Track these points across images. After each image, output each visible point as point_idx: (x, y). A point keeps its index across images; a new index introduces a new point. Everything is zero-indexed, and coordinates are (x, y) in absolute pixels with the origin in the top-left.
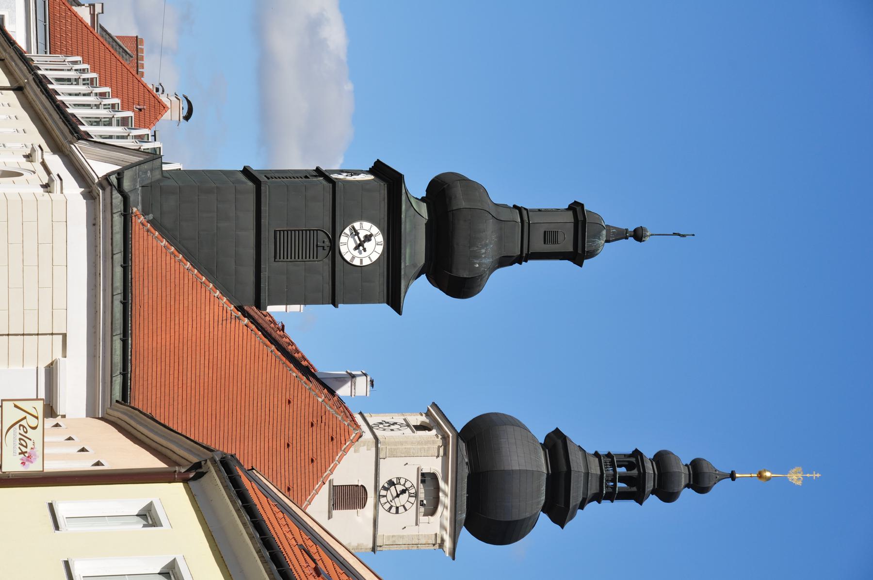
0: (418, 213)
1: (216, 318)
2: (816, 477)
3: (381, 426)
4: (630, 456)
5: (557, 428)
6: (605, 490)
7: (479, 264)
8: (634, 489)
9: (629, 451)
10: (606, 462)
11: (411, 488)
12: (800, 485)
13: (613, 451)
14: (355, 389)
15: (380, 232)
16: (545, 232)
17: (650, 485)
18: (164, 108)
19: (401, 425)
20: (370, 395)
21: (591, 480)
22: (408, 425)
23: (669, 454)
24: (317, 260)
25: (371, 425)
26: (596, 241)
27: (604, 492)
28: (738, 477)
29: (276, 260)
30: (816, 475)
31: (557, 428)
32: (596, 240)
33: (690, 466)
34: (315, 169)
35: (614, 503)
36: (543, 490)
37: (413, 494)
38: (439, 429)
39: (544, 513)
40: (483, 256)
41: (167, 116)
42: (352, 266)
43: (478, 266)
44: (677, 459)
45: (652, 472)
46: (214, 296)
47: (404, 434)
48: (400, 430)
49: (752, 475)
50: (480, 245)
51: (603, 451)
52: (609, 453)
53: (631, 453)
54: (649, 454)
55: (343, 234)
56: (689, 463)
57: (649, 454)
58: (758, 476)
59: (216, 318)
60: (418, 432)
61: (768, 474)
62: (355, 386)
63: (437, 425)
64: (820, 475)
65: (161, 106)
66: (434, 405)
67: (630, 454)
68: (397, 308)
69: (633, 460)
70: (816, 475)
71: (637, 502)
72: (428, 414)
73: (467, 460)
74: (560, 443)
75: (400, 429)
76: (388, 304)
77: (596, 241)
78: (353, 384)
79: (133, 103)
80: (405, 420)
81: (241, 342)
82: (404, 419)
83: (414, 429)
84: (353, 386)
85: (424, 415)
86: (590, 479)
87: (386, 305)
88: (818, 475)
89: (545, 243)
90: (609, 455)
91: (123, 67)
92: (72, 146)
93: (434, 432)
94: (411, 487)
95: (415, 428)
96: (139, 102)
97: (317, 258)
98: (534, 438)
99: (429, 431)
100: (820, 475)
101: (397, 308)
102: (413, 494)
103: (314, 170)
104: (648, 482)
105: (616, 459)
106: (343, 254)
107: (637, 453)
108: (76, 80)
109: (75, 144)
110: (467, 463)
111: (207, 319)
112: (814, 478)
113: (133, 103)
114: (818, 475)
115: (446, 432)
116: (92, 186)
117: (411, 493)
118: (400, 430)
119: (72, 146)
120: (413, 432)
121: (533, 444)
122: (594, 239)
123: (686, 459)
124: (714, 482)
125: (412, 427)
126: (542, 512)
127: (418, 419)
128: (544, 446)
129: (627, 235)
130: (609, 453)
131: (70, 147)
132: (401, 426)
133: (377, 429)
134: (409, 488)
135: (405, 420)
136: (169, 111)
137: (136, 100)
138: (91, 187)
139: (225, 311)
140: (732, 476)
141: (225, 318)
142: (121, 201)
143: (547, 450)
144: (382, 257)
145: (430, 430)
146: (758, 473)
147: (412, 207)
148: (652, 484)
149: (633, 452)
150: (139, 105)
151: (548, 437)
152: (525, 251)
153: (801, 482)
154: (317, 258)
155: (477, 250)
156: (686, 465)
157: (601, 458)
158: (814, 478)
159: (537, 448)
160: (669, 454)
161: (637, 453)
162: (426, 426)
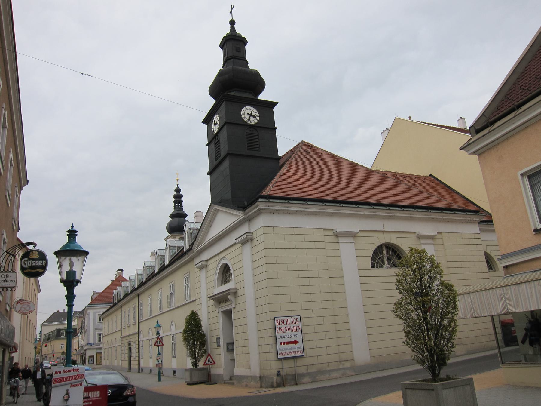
119: (195, 251)
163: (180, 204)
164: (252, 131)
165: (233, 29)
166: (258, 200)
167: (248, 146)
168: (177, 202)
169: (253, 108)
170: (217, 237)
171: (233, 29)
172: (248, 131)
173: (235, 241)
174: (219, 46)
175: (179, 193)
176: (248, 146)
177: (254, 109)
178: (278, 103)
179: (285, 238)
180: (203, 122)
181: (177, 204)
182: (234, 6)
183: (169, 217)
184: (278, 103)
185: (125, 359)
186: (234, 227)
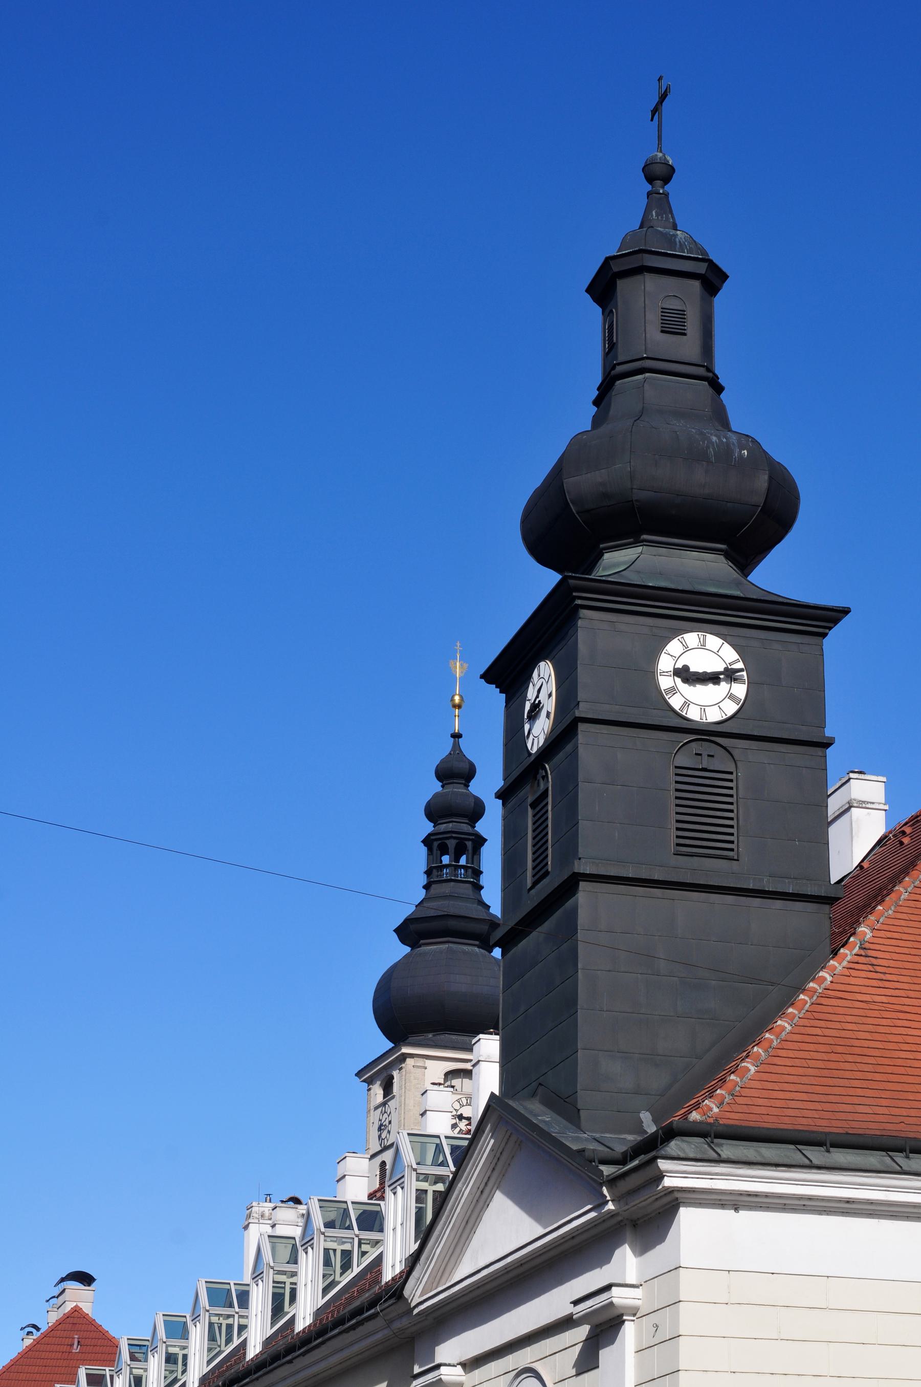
0: (631, 565)
1: (875, 983)
2: (460, 647)
3: (383, 1136)
4: (430, 850)
5: (394, 931)
6: (469, 879)
7: (742, 449)
8: (469, 844)
9: (424, 850)
10: (438, 876)
11: (461, 1102)
12: (467, 665)
13: (424, 868)
14: (873, 803)
15: (679, 637)
16: (662, 332)
17: (466, 828)
18: (76, 1311)
19: (383, 1113)
20: (883, 776)
21: (457, 894)
22: (384, 1104)
23: (429, 804)
24: (735, 773)
25: (380, 1149)
26: (680, 242)
27: (472, 880)
28: (458, 730)
29: (736, 857)
30: (458, 646)
31: (394, 931)
32: (677, 240)
33: (444, 782)
34: (501, 801)
35: (484, 871)
36: (467, 949)
37: (467, 1100)
38: (392, 1066)
39: (492, 952)
40: (724, 440)
41: (87, 1308)
42: (726, 723)
43: (746, 452)
44: (436, 796)
45: (451, 824)
46: (832, 982)
47: (396, 1109)
48: (390, 1113)
49: (457, 715)
50: (704, 443)
51: (423, 880)
52: (425, 873)
53: (426, 848)
54: (428, 827)
55: (684, 714)
56: (441, 784)
57: (428, 827)
58: (458, 709)
59: (875, 983)
60: (394, 1092)
61: (457, 699)
62: (868, 803)
63: (386, 1070)
64: (458, 642)
65: (73, 1315)
66: (359, 1074)
67: (428, 850)
68: (835, 615)
69: (436, 844)
70: (458, 646)
71: (483, 845)
72: (370, 1082)
73: (430, 1035)
74: (412, 927)
75: (388, 1113)
76: (824, 635)
77: (680, 242)
78: (864, 805)
79: (69, 1353)
80: (376, 1108)
81: (909, 944)
82: (374, 1111)
83: (387, 1098)
84: (867, 806)
85: (371, 1086)
86: (456, 895)
87: (826, 641)
88: (458, 644)
89: (685, 334)
90: (428, 873)
91: (18, 1363)
92: (416, 1311)
93: (395, 1073)
94: (459, 1102)
95: (388, 1095)
96: (68, 1345)
97: (731, 773)
98: (406, 956)
99: (393, 1079)
100: (458, 642)
101: (835, 615)
102: (467, 1100)
103: (503, 804)
104: (462, 830)
105: (433, 864)
106: (725, 717)
107: (427, 842)
108: (170, 1359)
109: (413, 1305)
110: (434, 1036)
111: (884, 999)
112: (462, 649)
113: (69, 1353)
114: (458, 644)
115: (396, 1057)
116: (620, 1218)
117: (467, 1103)
118: (390, 1113)
119: (416, 1311)
120: (394, 1097)
121: (413, 957)
122: (676, 244)
123: (436, 787)
124: (464, 757)
125: (385, 1100)
126: (492, 954)
127: (377, 1092)
128: (414, 945)
129: (661, 192)
130: (425, 873)
131: (419, 1314)
132: (385, 1112)
133: (388, 1140)
134: (460, 1104)
135: (376, 1108)
136: (81, 1305)
137: (65, 1348)
138: (621, 1221)
139: (856, 966)
140: (457, 736)
141: (870, 968)
142: (683, 1141)
143: (422, 941)
144: (729, 638)
145: (392, 1077)
146: (454, 709)
147: (622, 573)
148: (465, 825)
149: (425, 845)
150: (72, 1345)
151: (403, 941)
152: (701, 371)
153: (465, 664)
154: (731, 773)
155: (714, 449)
156: (443, 786)
157: (432, 882)
158: (462, 649)
159: (418, 953)
160: (429, 804)
161: (427, 842)
162: (385, 1083)
163: (463, 861)
164: (705, 757)
165: (456, 747)
166: (663, 1152)
167: (680, 833)
168: (452, 844)
169: (720, 641)
170: (505, 1267)
171: (456, 747)
172: (683, 760)
173: (569, 1309)
174: (589, 290)
175: (461, 790)
176: (680, 833)
177: (727, 646)
178: (846, 611)
179: (771, 1374)
180: (490, 676)
181: (446, 860)
182: (652, 120)
183: (395, 936)
184: (846, 611)
185: (259, 1204)
186: (573, 1237)
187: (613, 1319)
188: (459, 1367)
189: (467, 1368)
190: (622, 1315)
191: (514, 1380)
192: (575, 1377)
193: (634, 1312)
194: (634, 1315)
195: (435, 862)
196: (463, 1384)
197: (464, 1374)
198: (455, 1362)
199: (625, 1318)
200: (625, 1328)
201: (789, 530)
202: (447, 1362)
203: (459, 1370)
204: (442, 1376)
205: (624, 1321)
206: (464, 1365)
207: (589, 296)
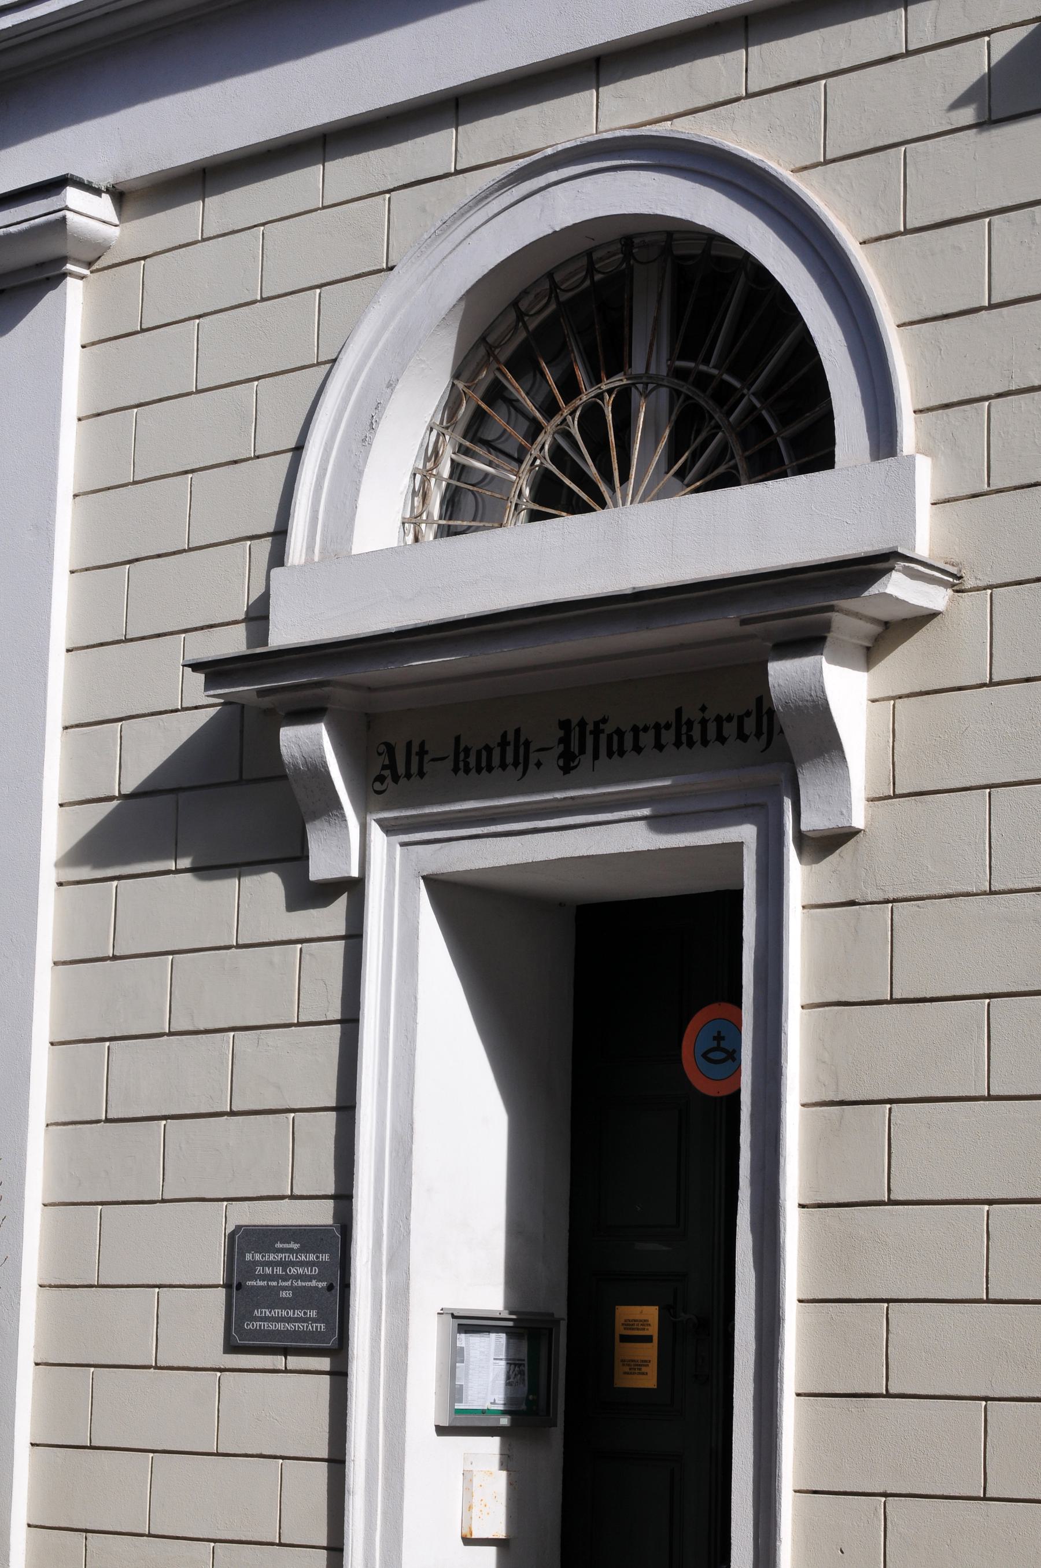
187: (40, 265)
188: (106, 198)
189: (129, 209)
190: (64, 260)
191: (497, 190)
192: (974, 130)
193: (90, 257)
194: (89, 264)
195: (478, 518)
196: (109, 248)
197: (117, 222)
198: (102, 180)
199: (70, 267)
200: (66, 285)
201: (719, 476)
202: (86, 178)
203: (104, 206)
204: (69, 215)
205: (64, 275)
206: (120, 196)
207: (836, 449)
